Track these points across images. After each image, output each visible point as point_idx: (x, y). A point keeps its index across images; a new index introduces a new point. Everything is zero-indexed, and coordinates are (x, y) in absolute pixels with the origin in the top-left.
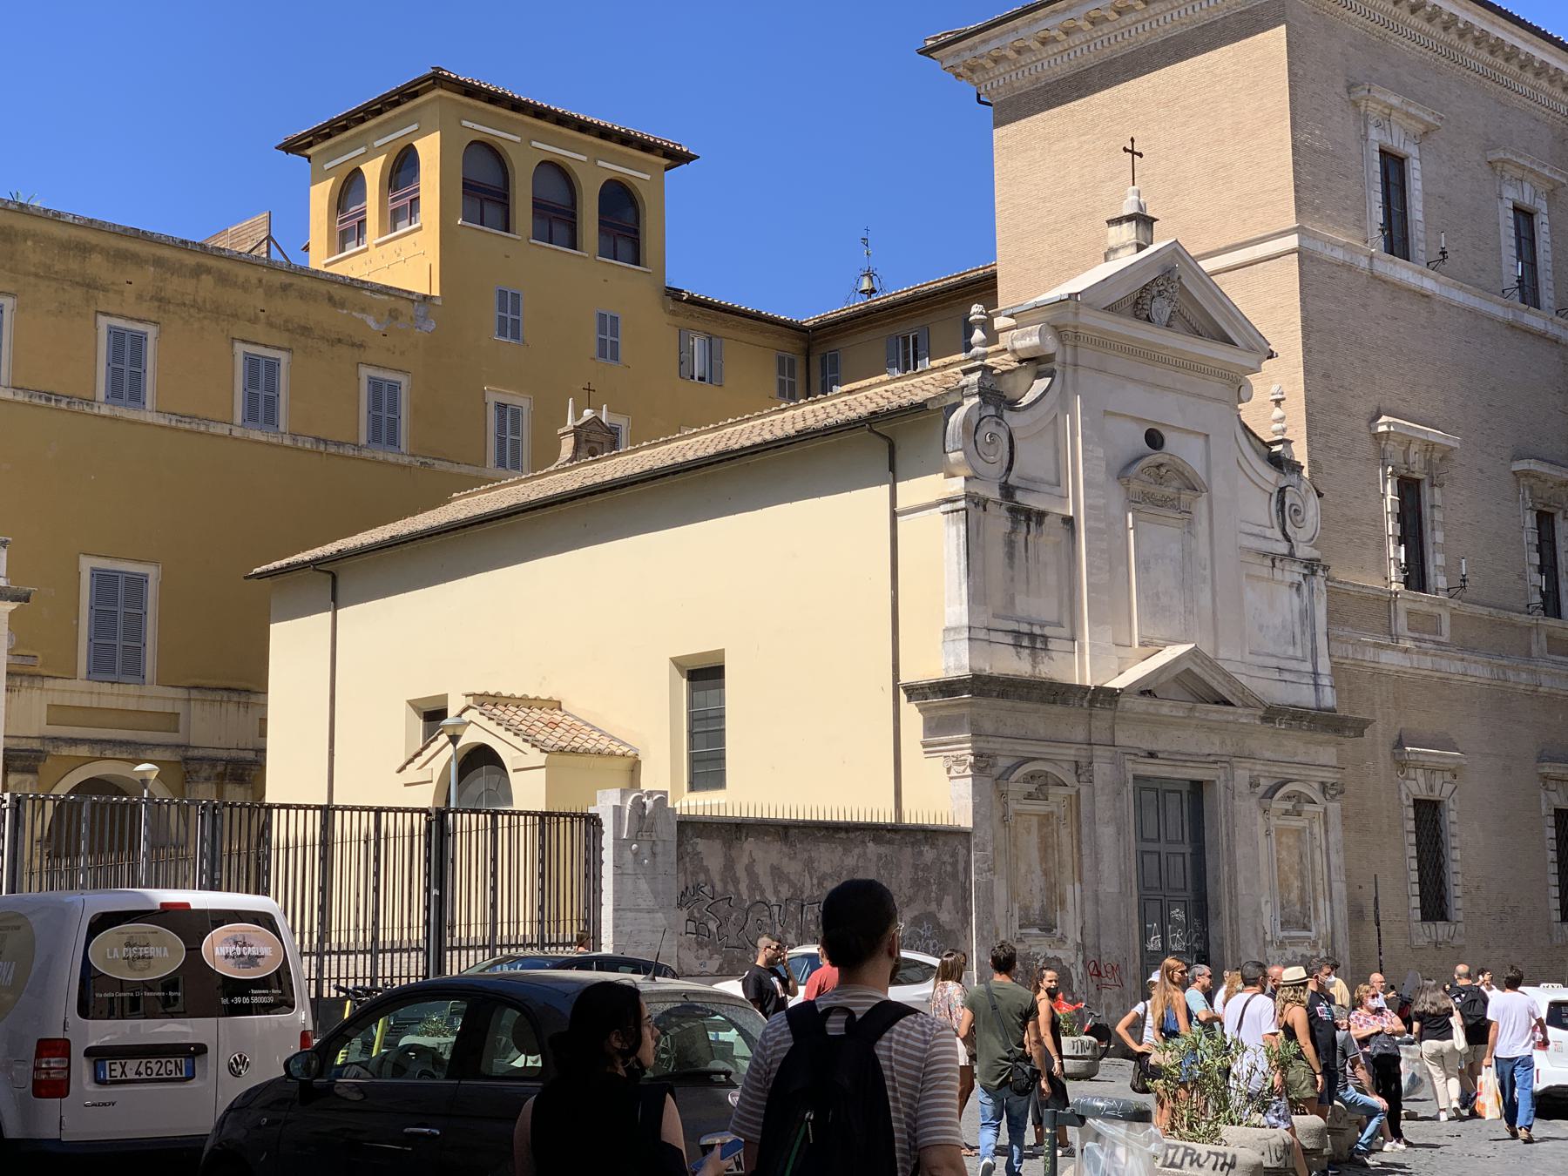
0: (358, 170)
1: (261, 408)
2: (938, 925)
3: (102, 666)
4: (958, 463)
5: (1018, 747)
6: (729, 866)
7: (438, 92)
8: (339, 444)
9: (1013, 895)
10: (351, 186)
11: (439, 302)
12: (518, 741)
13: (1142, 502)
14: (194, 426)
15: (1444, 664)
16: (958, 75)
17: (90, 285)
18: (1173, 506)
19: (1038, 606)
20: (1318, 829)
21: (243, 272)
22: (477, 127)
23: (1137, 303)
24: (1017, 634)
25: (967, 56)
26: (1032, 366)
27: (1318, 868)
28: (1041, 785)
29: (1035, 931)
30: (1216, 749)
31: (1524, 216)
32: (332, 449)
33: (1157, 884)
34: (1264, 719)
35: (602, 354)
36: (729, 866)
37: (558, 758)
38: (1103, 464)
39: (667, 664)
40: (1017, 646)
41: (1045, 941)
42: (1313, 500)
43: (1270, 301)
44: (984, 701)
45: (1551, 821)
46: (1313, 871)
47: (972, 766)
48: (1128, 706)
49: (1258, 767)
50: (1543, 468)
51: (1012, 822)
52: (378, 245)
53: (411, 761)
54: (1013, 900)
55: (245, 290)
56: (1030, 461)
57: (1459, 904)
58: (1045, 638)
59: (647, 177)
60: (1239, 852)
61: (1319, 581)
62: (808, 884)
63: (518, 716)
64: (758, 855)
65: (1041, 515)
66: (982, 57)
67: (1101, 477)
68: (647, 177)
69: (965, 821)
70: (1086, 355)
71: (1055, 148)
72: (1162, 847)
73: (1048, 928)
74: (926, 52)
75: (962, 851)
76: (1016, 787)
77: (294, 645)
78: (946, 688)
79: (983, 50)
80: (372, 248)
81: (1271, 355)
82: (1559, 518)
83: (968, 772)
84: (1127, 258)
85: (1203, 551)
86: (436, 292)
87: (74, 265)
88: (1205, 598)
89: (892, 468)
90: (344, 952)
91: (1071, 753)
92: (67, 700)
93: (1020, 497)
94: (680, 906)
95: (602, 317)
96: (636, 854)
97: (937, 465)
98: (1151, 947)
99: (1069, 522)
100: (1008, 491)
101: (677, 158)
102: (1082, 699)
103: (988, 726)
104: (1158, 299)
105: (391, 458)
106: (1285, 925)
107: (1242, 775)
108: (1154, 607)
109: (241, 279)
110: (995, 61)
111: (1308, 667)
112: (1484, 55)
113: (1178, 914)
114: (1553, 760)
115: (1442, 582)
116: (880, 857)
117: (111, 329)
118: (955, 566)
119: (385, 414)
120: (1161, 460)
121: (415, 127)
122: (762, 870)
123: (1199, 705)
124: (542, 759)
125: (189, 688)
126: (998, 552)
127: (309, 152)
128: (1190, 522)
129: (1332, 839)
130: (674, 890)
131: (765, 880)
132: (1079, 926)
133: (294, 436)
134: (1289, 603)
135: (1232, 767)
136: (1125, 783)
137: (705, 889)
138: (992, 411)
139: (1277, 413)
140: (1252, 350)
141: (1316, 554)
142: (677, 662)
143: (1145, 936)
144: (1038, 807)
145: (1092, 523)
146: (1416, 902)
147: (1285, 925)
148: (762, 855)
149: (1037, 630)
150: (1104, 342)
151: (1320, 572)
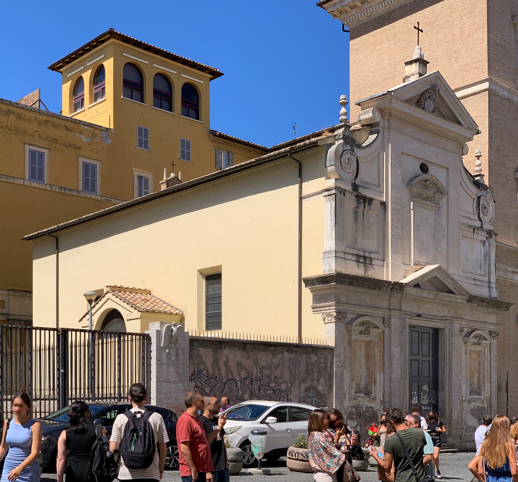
0: (81, 77)
1: (37, 173)
2: (318, 392)
4: (332, 172)
5: (358, 310)
6: (216, 361)
7: (113, 40)
8: (70, 190)
9: (352, 379)
10: (78, 83)
11: (113, 131)
12: (128, 307)
13: (419, 198)
14: (8, 180)
16: (335, 16)
18: (431, 201)
19: (369, 244)
20: (487, 351)
21: (28, 114)
22: (129, 56)
23: (418, 101)
24: (358, 256)
27: (486, 368)
28: (367, 327)
29: (362, 395)
30: (446, 314)
32: (68, 192)
33: (417, 374)
35: (183, 157)
36: (216, 361)
37: (146, 314)
38: (400, 178)
39: (196, 273)
40: (358, 261)
41: (366, 399)
42: (492, 203)
43: (478, 110)
44: (342, 287)
46: (484, 370)
47: (335, 317)
48: (408, 292)
49: (464, 323)
51: (353, 344)
52: (89, 108)
53: (84, 317)
54: (352, 380)
55: (29, 122)
56: (366, 174)
58: (371, 259)
59: (202, 82)
60: (454, 361)
61: (493, 241)
62: (255, 371)
63: (129, 296)
64: (231, 356)
65: (371, 200)
66: (346, 6)
68: (202, 82)
69: (331, 343)
71: (377, 48)
72: (420, 358)
73: (368, 393)
74: (320, 5)
75: (329, 357)
76: (356, 328)
77: (42, 268)
78: (324, 280)
80: (87, 110)
83: (334, 320)
85: (444, 223)
86: (112, 127)
88: (444, 244)
90: (52, 399)
91: (381, 313)
93: (361, 190)
94: (191, 380)
95: (183, 141)
96: (168, 354)
97: (323, 174)
98: (413, 402)
99: (384, 204)
100: (355, 187)
101: (215, 75)
102: (387, 287)
103: (343, 299)
104: (428, 100)
105: (93, 197)
107: (456, 326)
108: (421, 248)
109: (27, 117)
110: (351, 8)
111: (486, 279)
113: (425, 388)
116: (290, 359)
118: (329, 222)
120: (427, 178)
121: (103, 56)
123: (441, 293)
124: (138, 315)
125: (8, 290)
126: (350, 216)
127: (62, 70)
128: (439, 209)
129: (492, 355)
130: (188, 372)
131: (234, 369)
132: (382, 392)
133: (51, 186)
134: (479, 250)
135: (453, 323)
136: (405, 328)
137: (204, 372)
138: (349, 147)
139: (478, 162)
140: (469, 128)
141: (492, 228)
142: (200, 272)
143: (411, 397)
145: (394, 206)
147: (471, 393)
148: (233, 357)
149: (367, 255)
150: (403, 119)
151: (494, 236)
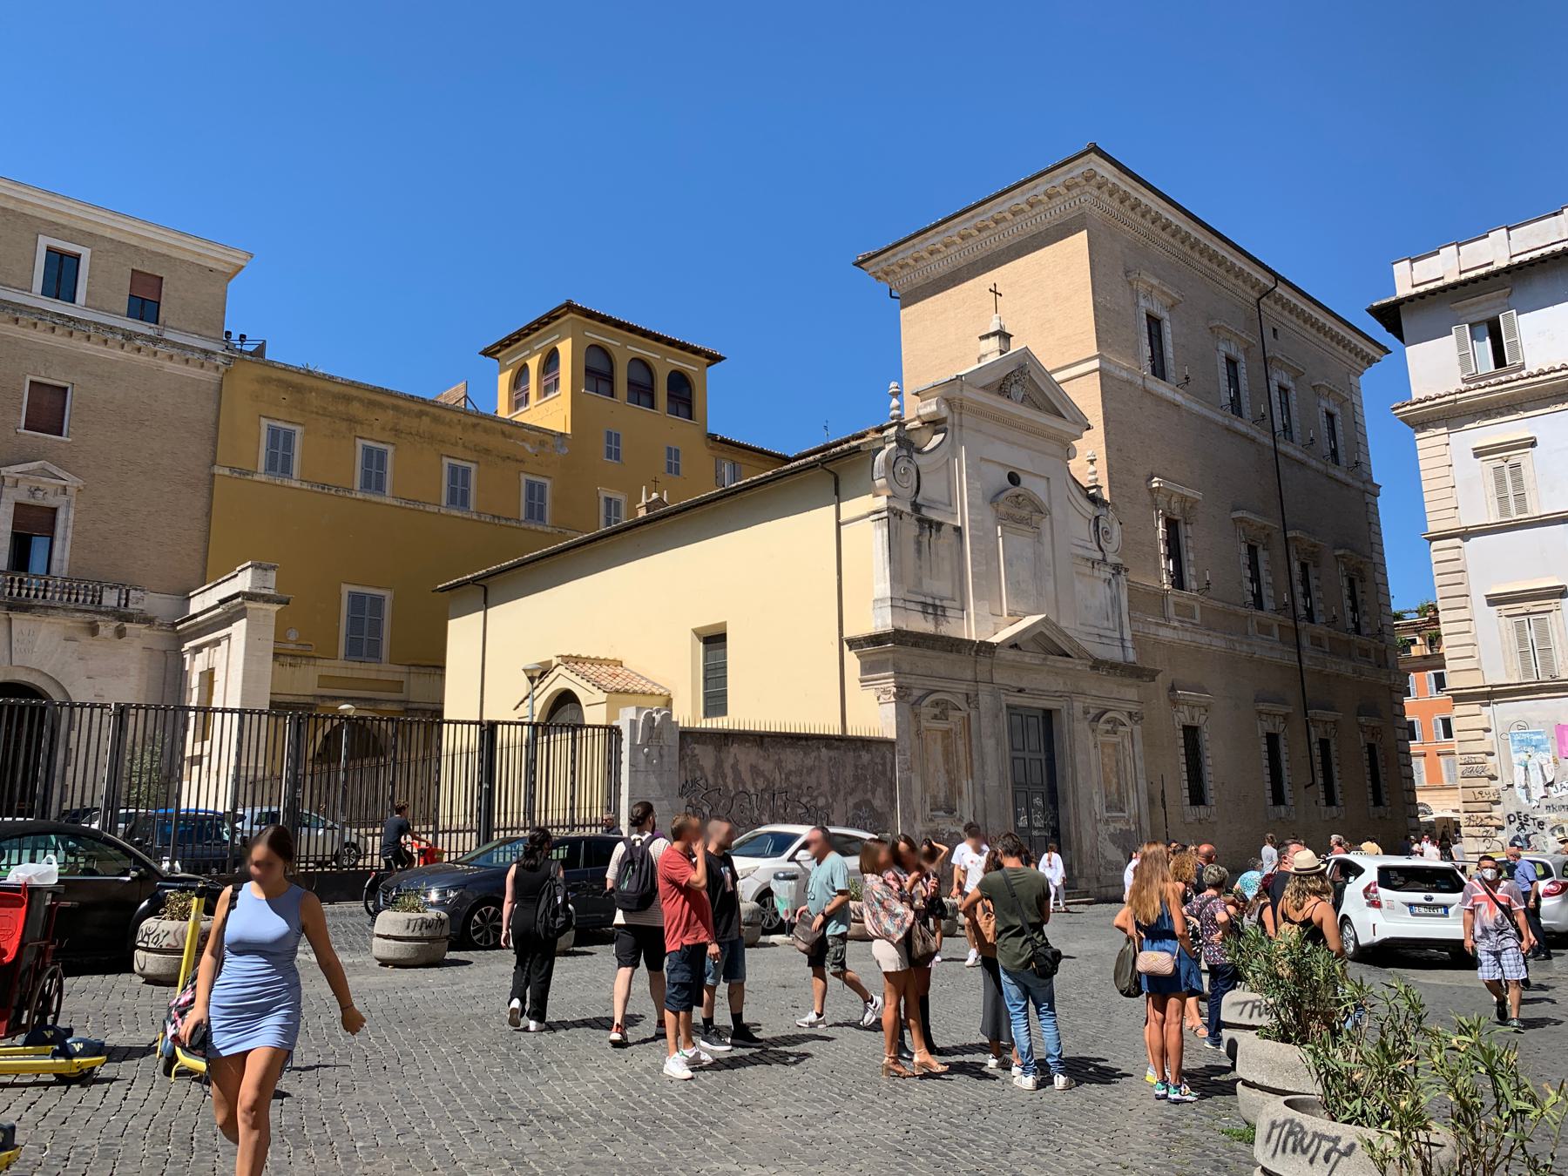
1: (459, 496)
2: (873, 809)
3: (354, 651)
4: (882, 487)
6: (719, 764)
7: (571, 315)
10: (521, 375)
12: (589, 686)
15: (1198, 638)
16: (878, 278)
17: (351, 420)
19: (940, 587)
21: (449, 416)
24: (924, 604)
25: (884, 265)
26: (932, 427)
30: (1061, 688)
31: (1231, 363)
34: (1092, 668)
35: (670, 471)
36: (719, 764)
41: (949, 821)
42: (1116, 526)
43: (1087, 397)
44: (902, 649)
45: (1264, 740)
50: (1252, 517)
56: (930, 489)
57: (1212, 794)
58: (944, 608)
61: (1122, 578)
63: (590, 670)
64: (741, 757)
65: (940, 525)
67: (979, 501)
70: (967, 419)
73: (950, 811)
74: (858, 264)
75: (889, 756)
76: (926, 710)
77: (462, 633)
78: (876, 640)
79: (893, 260)
81: (1089, 428)
82: (1260, 549)
84: (995, 357)
85: (1048, 554)
87: (341, 408)
88: (1050, 586)
89: (837, 493)
91: (963, 687)
92: (331, 673)
93: (924, 511)
94: (681, 795)
96: (647, 756)
99: (958, 530)
100: (916, 507)
101: (715, 359)
103: (906, 667)
105: (540, 528)
106: (1109, 808)
108: (1016, 591)
112: (1205, 261)
113: (1038, 801)
114: (1264, 701)
115: (1194, 585)
117: (364, 447)
119: (536, 502)
122: (742, 767)
128: (1039, 535)
131: (746, 776)
133: (479, 514)
134: (1102, 593)
138: (905, 452)
139: (1092, 468)
140: (1076, 423)
141: (1120, 561)
142: (696, 632)
143: (1017, 818)
144: (941, 725)
146: (1186, 793)
147: (1109, 808)
149: (938, 602)
150: (981, 412)
